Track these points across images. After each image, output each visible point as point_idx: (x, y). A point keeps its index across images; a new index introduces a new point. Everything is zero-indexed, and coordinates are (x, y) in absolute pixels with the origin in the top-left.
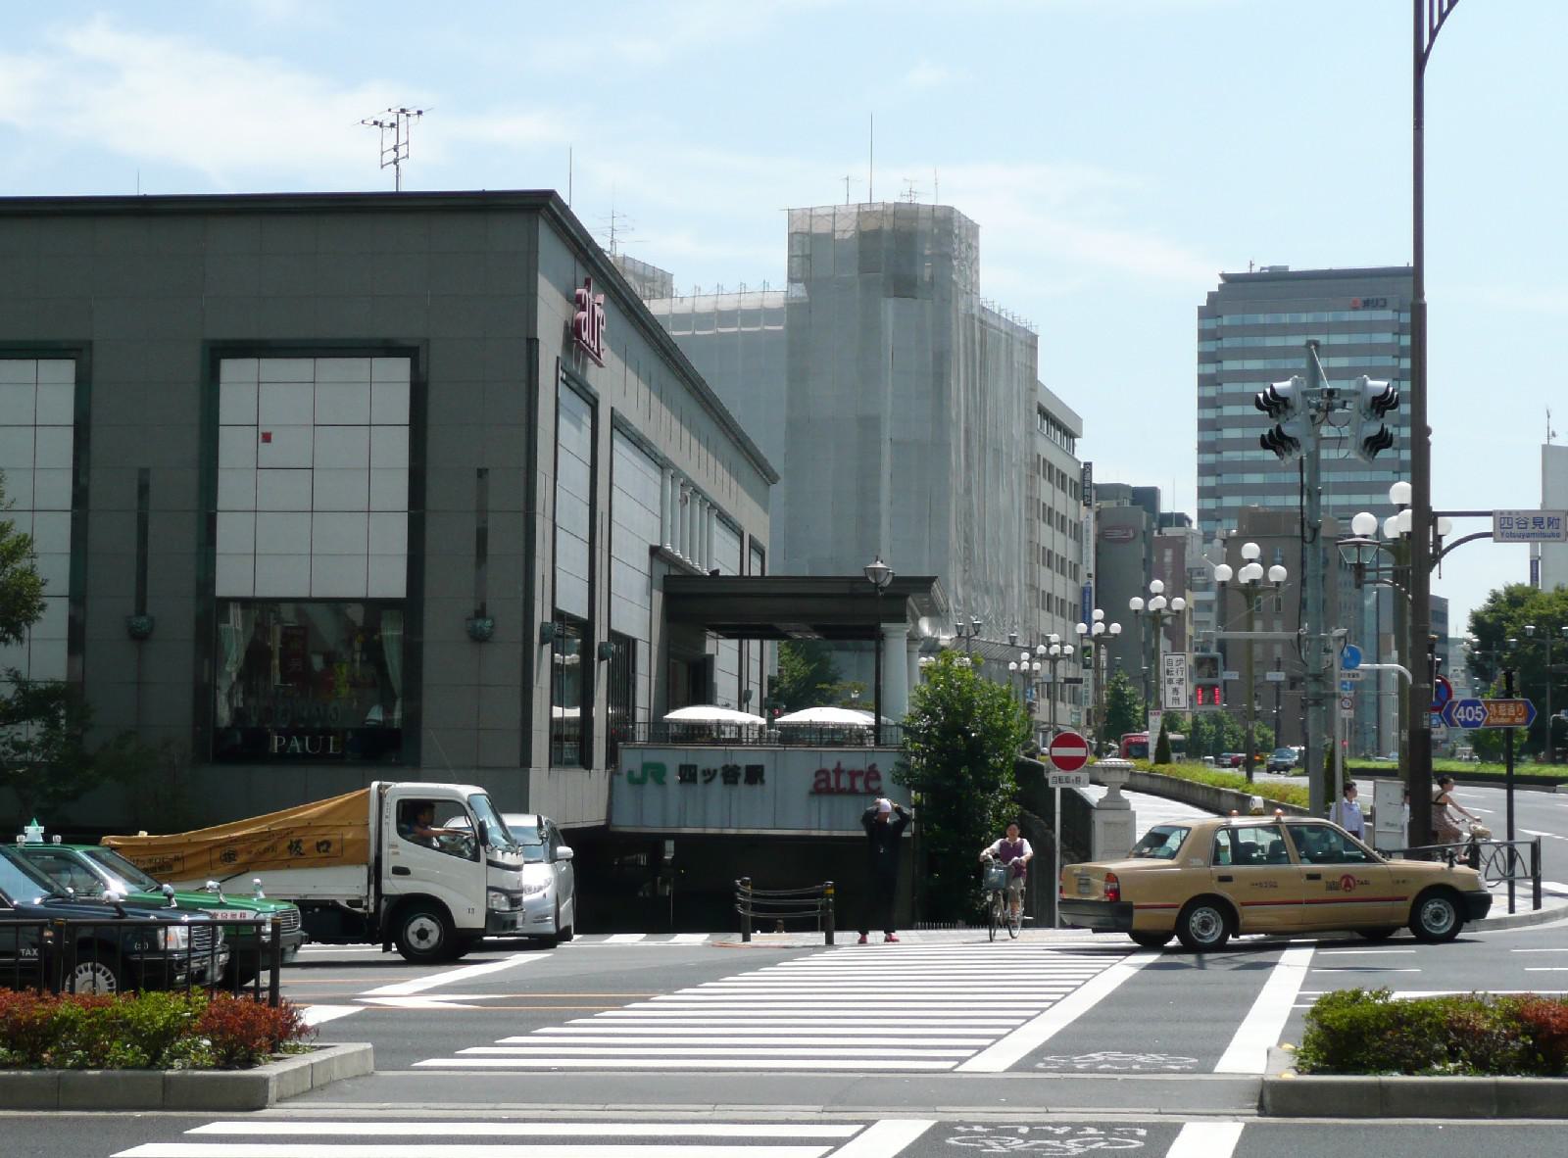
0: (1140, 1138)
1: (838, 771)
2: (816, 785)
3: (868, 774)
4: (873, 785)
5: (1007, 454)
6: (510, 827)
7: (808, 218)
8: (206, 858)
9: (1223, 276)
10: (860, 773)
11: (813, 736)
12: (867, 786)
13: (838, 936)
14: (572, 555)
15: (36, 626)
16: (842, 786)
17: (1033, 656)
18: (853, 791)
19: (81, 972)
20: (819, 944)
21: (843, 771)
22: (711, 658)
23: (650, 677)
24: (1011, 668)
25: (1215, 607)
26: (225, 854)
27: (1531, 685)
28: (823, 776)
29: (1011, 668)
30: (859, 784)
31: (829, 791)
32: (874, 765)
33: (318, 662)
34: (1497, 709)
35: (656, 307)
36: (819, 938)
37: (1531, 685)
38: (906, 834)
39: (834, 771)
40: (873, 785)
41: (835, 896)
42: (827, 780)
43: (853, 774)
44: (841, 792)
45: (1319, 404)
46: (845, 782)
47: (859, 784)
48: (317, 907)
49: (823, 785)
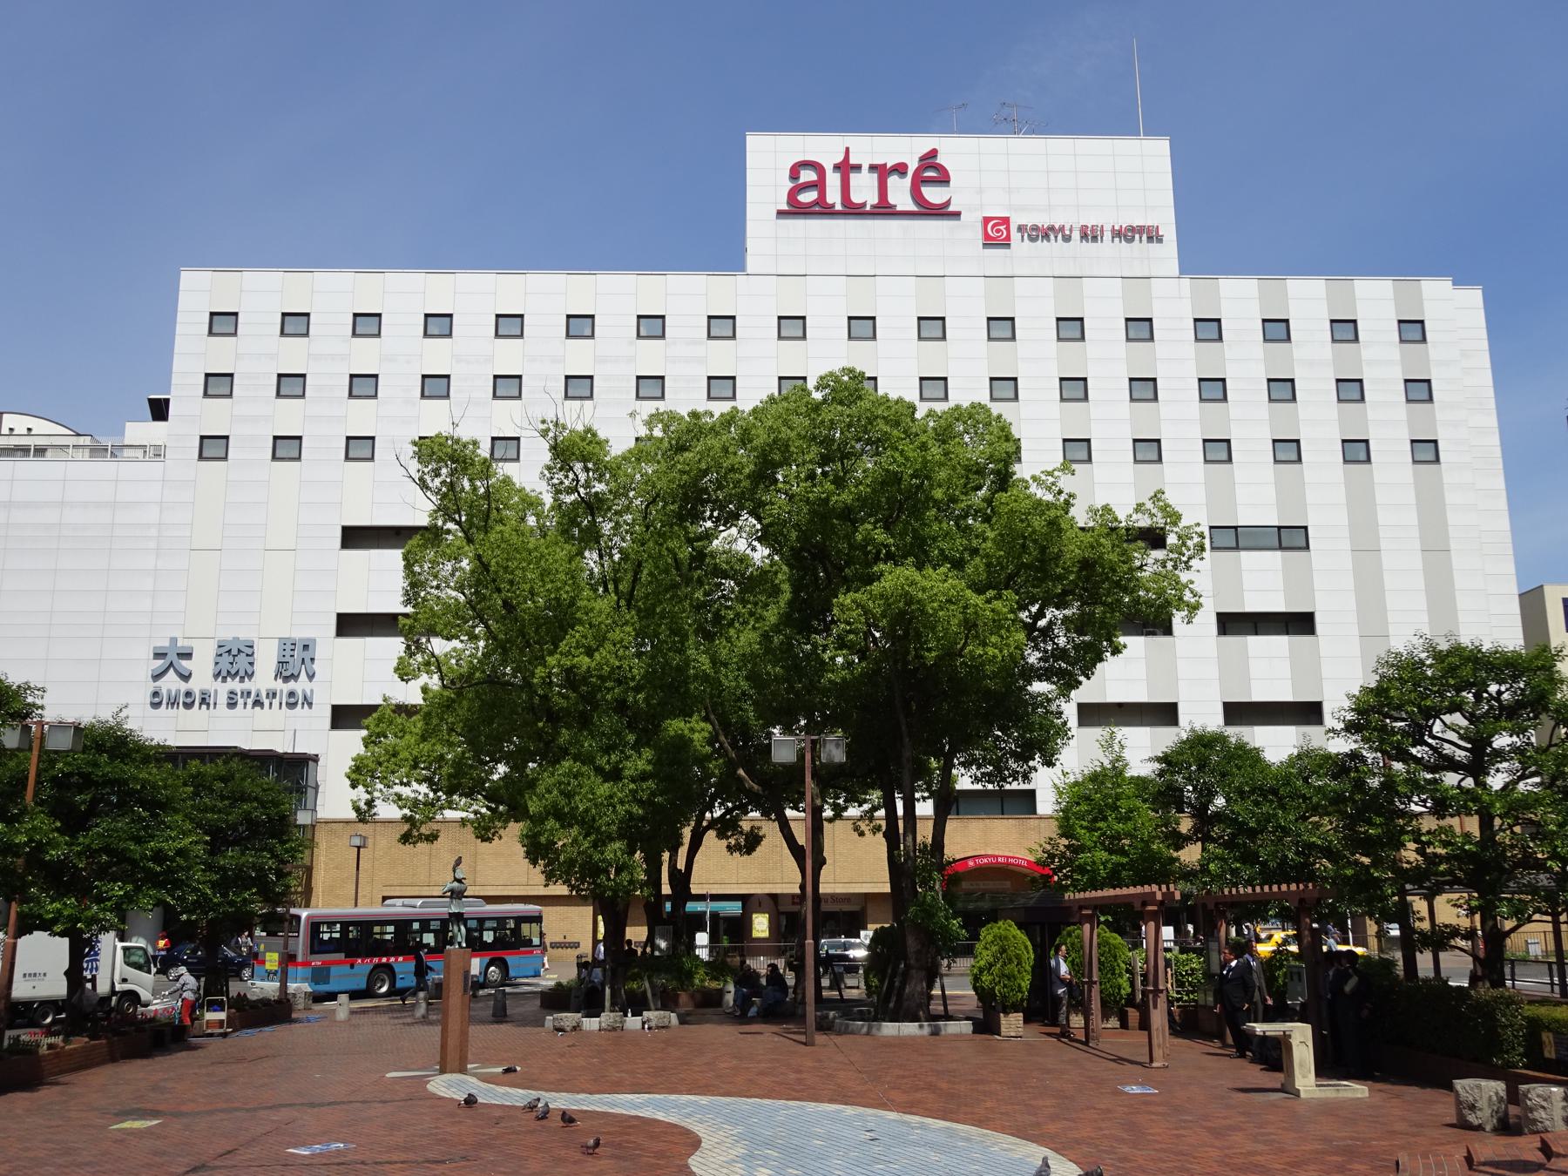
0: (1230, 892)
1: (846, 168)
2: (792, 196)
4: (933, 195)
9: (732, 854)
10: (900, 169)
13: (1262, 1034)
14: (1277, 1033)
15: (514, 480)
17: (1440, 807)
18: (884, 210)
21: (858, 168)
25: (279, 974)
27: (1365, 1013)
28: (808, 176)
31: (822, 210)
32: (933, 153)
35: (868, 208)
36: (1267, 1034)
37: (1365, 1013)
39: (837, 167)
40: (933, 195)
42: (820, 185)
43: (882, 172)
44: (852, 210)
49: (808, 197)
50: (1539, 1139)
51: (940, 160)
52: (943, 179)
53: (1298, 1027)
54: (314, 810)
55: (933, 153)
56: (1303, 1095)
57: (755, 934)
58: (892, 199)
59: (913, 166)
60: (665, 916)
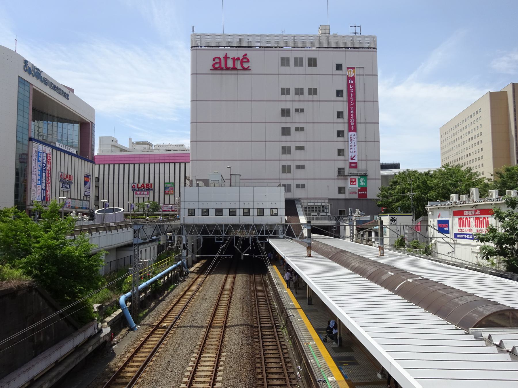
1: (226, 58)
2: (213, 65)
3: (243, 59)
4: (246, 65)
6: (225, 179)
8: (259, 287)
10: (238, 59)
16: (228, 66)
18: (234, 68)
19: (12, 207)
22: (424, 172)
23: (238, 74)
24: (140, 315)
26: (403, 188)
28: (217, 60)
29: (140, 315)
30: (238, 65)
40: (246, 65)
42: (220, 63)
43: (234, 59)
44: (228, 69)
45: (450, 177)
46: (230, 64)
47: (238, 65)
49: (217, 66)
52: (248, 61)
55: (246, 55)
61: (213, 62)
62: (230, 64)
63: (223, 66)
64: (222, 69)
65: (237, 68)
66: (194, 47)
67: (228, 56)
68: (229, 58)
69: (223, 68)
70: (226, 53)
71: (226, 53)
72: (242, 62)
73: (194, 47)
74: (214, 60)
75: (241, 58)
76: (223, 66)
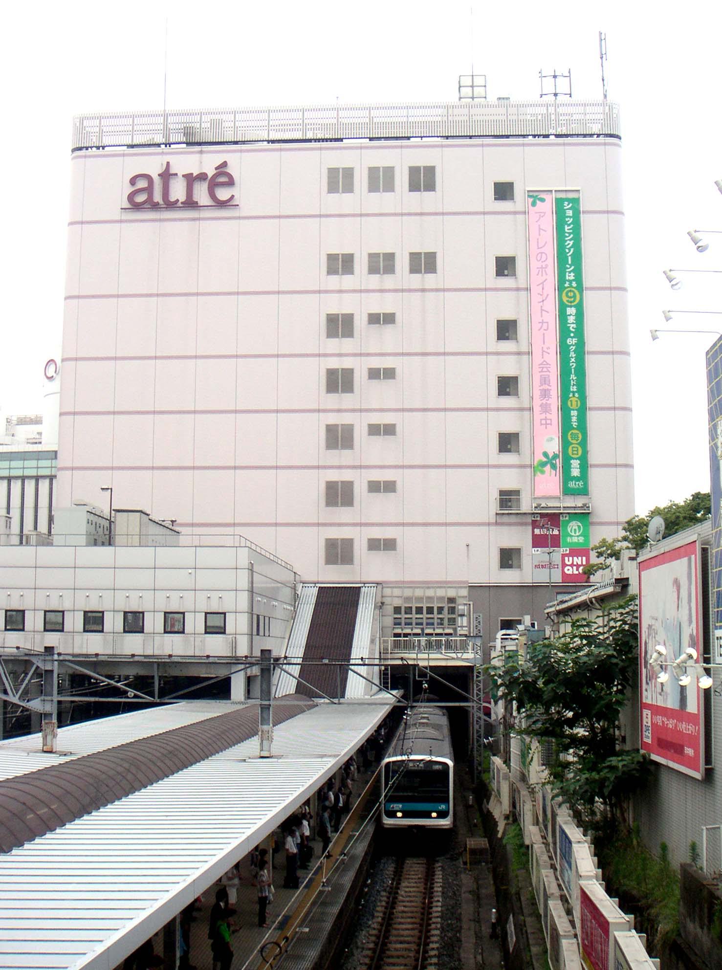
1: (167, 175)
2: (131, 197)
4: (223, 194)
5: (704, 925)
7: (659, 849)
10: (202, 177)
11: (553, 710)
12: (212, 195)
18: (190, 204)
20: (398, 288)
28: (142, 184)
30: (201, 194)
32: (225, 164)
33: (617, 823)
34: (370, 949)
36: (700, 524)
38: (92, 680)
40: (223, 194)
41: (600, 683)
42: (149, 190)
43: (190, 179)
44: (171, 205)
47: (201, 194)
48: (434, 818)
49: (141, 198)
50: (258, 674)
51: (229, 170)
52: (231, 183)
53: (204, 674)
54: (426, 628)
55: (225, 164)
56: (59, 730)
57: (613, 590)
58: (196, 198)
59: (211, 173)
60: (609, 819)
61: (130, 189)
62: (178, 192)
63: (158, 197)
64: (155, 207)
65: (197, 203)
66: (80, 149)
67: (172, 171)
68: (176, 174)
69: (158, 203)
70: (168, 163)
71: (168, 163)
72: (213, 185)
73: (80, 149)
74: (133, 181)
75: (210, 175)
76: (158, 197)
